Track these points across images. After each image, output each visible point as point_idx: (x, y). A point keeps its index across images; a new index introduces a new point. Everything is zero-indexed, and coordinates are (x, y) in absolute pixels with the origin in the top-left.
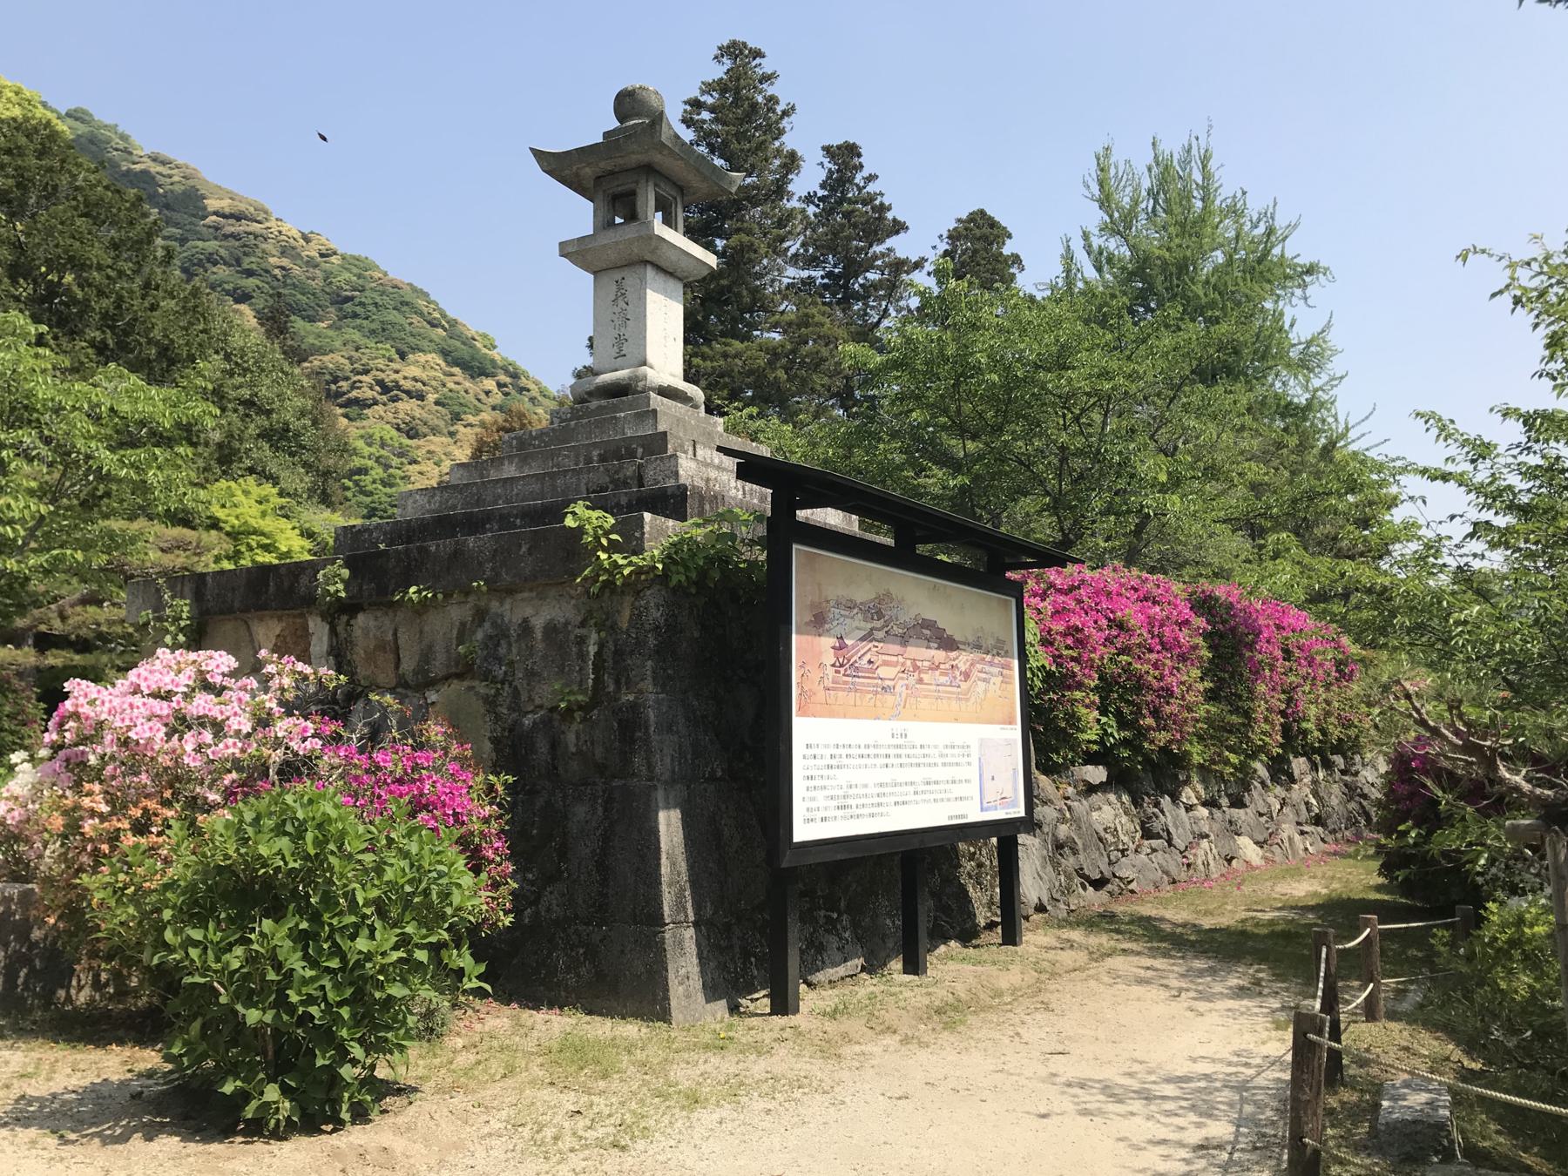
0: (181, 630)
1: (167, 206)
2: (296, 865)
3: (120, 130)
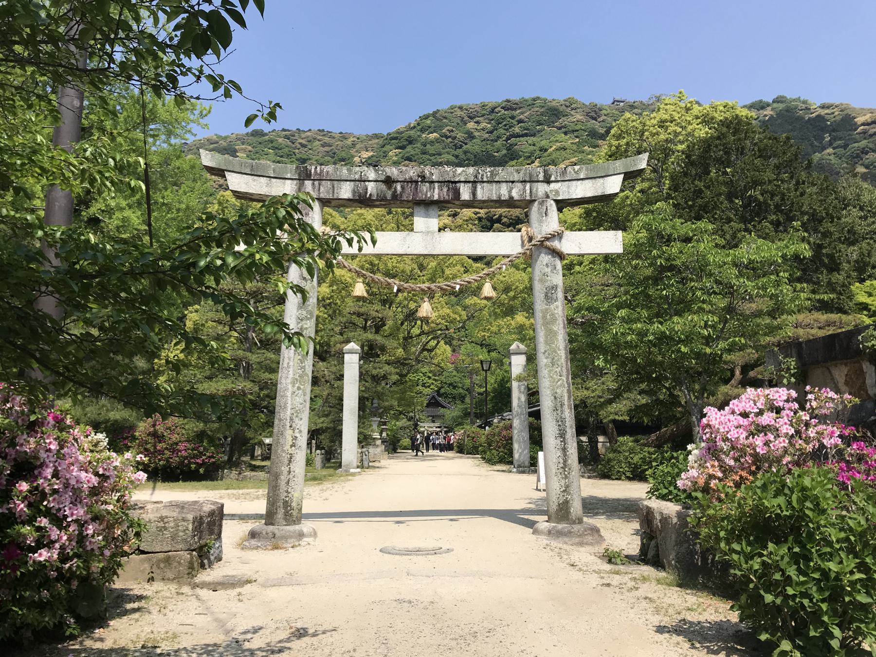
0: (793, 375)
1: (834, 130)
2: (788, 514)
3: (802, 99)
